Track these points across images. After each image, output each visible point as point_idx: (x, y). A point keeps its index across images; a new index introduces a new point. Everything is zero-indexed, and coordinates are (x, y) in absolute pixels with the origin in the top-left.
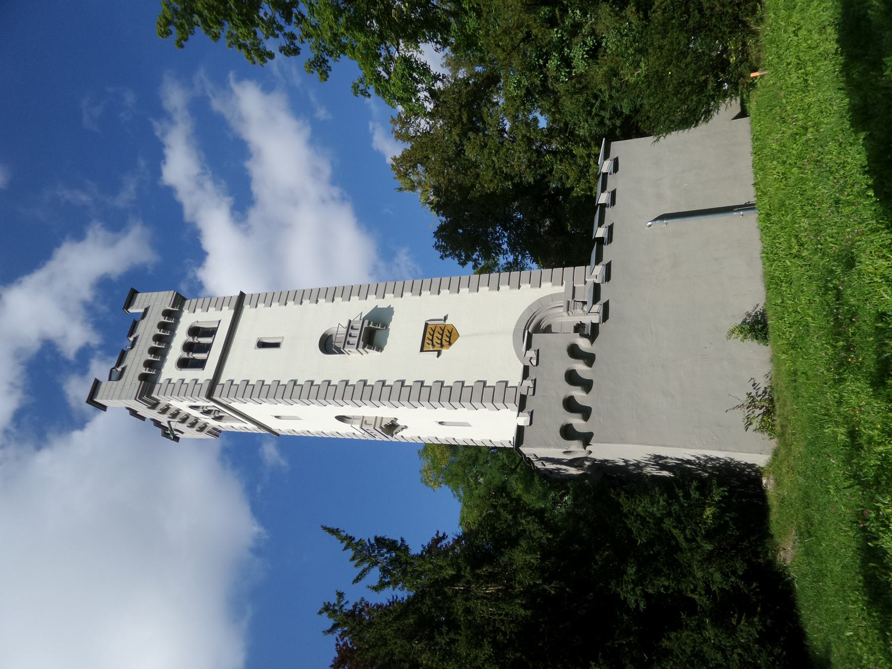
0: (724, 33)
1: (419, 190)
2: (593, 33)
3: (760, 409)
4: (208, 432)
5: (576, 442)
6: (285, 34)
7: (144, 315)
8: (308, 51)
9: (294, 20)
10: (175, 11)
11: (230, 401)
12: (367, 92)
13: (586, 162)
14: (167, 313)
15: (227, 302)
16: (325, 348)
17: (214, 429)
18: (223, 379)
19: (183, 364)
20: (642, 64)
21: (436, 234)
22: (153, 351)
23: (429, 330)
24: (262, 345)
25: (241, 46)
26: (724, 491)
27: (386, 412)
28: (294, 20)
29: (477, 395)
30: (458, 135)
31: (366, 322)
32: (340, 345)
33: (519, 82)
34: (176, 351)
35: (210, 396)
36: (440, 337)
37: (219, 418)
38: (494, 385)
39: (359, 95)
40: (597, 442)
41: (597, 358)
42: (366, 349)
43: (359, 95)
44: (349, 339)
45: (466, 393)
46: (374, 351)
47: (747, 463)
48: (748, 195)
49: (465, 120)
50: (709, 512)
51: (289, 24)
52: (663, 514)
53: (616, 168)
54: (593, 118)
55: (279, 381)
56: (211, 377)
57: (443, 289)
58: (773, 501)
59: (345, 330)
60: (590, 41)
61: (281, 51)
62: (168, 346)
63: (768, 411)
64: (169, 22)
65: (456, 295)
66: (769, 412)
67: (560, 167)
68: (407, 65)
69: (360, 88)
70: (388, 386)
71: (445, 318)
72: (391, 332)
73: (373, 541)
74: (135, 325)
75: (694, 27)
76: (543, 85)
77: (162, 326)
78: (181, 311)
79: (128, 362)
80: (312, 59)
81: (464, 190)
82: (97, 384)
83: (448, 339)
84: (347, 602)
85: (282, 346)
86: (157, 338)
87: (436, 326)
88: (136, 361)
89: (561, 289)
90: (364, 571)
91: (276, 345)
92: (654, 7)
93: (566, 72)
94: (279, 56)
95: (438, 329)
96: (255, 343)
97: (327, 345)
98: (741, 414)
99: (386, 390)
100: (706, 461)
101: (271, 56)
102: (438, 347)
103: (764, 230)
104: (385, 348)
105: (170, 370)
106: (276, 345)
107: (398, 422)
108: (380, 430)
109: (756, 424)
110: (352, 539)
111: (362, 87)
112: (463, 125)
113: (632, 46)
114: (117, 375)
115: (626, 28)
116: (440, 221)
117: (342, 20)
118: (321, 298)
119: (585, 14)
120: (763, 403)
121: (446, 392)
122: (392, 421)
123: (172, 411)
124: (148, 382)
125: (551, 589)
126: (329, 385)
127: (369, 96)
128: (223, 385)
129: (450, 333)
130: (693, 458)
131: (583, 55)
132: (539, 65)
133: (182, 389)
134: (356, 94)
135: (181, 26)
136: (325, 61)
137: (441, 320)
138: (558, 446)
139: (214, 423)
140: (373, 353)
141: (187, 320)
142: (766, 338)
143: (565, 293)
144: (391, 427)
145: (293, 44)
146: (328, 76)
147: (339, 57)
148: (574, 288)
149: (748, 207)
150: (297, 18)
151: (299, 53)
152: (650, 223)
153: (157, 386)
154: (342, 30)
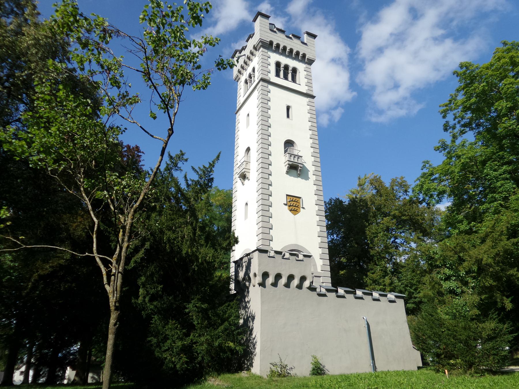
0: (466, 357)
1: (359, 189)
2: (463, 292)
3: (281, 371)
4: (238, 75)
5: (261, 280)
6: (455, 124)
7: (303, 43)
8: (447, 138)
9: (462, 129)
10: (473, 71)
11: (259, 90)
12: (424, 168)
13: (381, 283)
14: (304, 55)
15: (310, 88)
16: (288, 143)
17: (239, 79)
18: (271, 87)
19: (278, 64)
20: (447, 317)
21: (338, 199)
22: (285, 48)
23: (297, 199)
24: (288, 108)
25: (450, 101)
26: (241, 352)
27: (254, 174)
28: (462, 129)
29: (265, 225)
30: (395, 214)
31: (301, 166)
32: (288, 151)
33: (437, 254)
34: (284, 61)
35: (262, 80)
36: (294, 205)
37: (246, 82)
38: (271, 234)
39: (423, 164)
40: (261, 290)
41: (300, 290)
42: (288, 165)
43: (423, 164)
44: (293, 156)
45: (266, 219)
46: (286, 170)
47: (253, 363)
48: (381, 367)
49: (403, 218)
50: (231, 344)
51: (460, 126)
52: (230, 321)
53: (375, 300)
54: (403, 287)
55: (270, 118)
56: (271, 80)
57: (318, 207)
58: (237, 376)
59: (296, 154)
60: (459, 290)
61: (446, 122)
62: (287, 56)
63: (280, 374)
64: (467, 68)
65: (315, 214)
66: (280, 375)
67: (378, 269)
68: (441, 192)
69: (427, 165)
70: (269, 177)
71: (303, 208)
72: (296, 179)
73: (211, 177)
74: (298, 38)
75: (469, 343)
76: (435, 265)
77: (298, 53)
78: (306, 63)
79: (279, 34)
80: (446, 143)
81: (365, 217)
82: (267, 17)
83: (293, 209)
84: (183, 164)
85: (288, 119)
86: (291, 50)
87: (299, 203)
88: (280, 39)
89: (319, 270)
90: (197, 172)
91: (288, 116)
92: (478, 323)
93: (442, 278)
94: (444, 121)
95: (298, 204)
96: (289, 105)
97: (289, 144)
98: (277, 361)
99: (266, 176)
100: (252, 343)
101: (444, 117)
102: (289, 204)
103: (366, 374)
104: (288, 176)
105: (275, 57)
106: (288, 116)
107: (246, 181)
108: (243, 171)
109: (274, 368)
110: (213, 166)
111: (427, 166)
112: (400, 217)
113: (457, 312)
114: (272, 29)
115: (466, 309)
116: (345, 202)
117: (468, 160)
118: (313, 141)
119: (473, 288)
120: (283, 372)
121: (266, 208)
122: (248, 178)
123: (252, 57)
124: (268, 45)
125: (195, 267)
126: (269, 145)
127: (422, 169)
128: (267, 87)
129: (296, 211)
130: (253, 336)
131: (452, 287)
132: (446, 264)
133: (265, 64)
134: (424, 162)
135: (464, 73)
136: (445, 149)
137: (303, 206)
138: (259, 270)
139: (243, 78)
140: (285, 169)
141: (300, 66)
142: (313, 374)
143: (317, 272)
144: (243, 177)
145: (450, 128)
146: (436, 151)
147: (446, 156)
148: (320, 277)
149: (375, 368)
150: (463, 130)
151: (445, 131)
152: (365, 318)
153: (266, 51)
154: (462, 161)
